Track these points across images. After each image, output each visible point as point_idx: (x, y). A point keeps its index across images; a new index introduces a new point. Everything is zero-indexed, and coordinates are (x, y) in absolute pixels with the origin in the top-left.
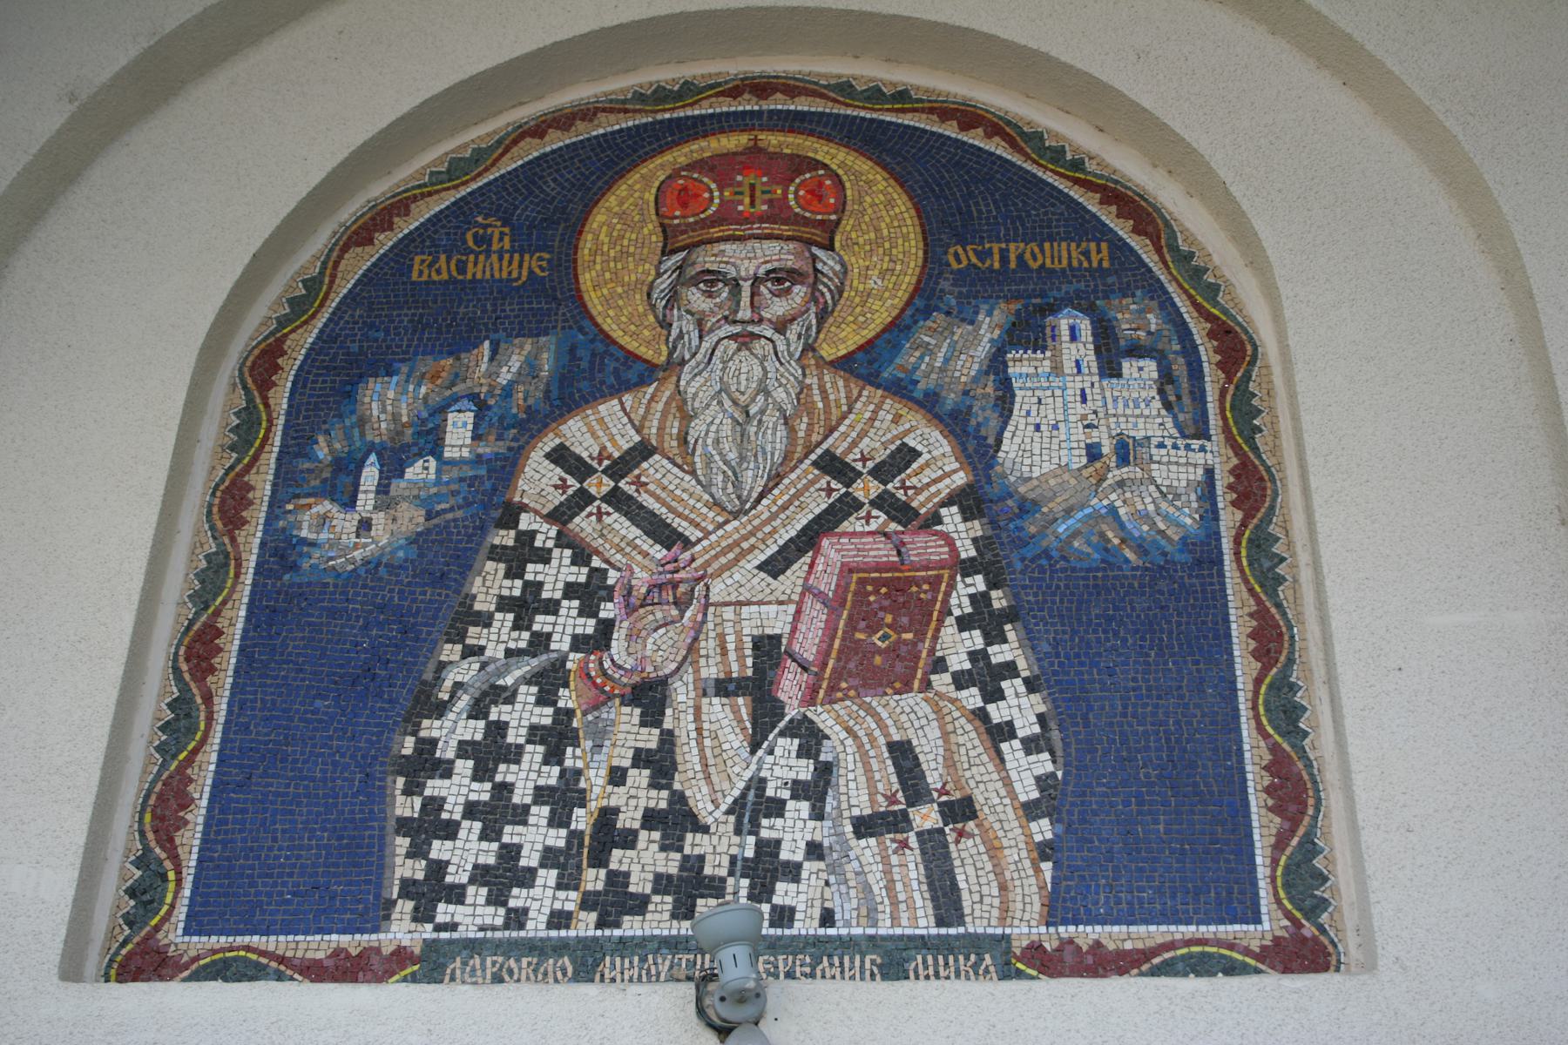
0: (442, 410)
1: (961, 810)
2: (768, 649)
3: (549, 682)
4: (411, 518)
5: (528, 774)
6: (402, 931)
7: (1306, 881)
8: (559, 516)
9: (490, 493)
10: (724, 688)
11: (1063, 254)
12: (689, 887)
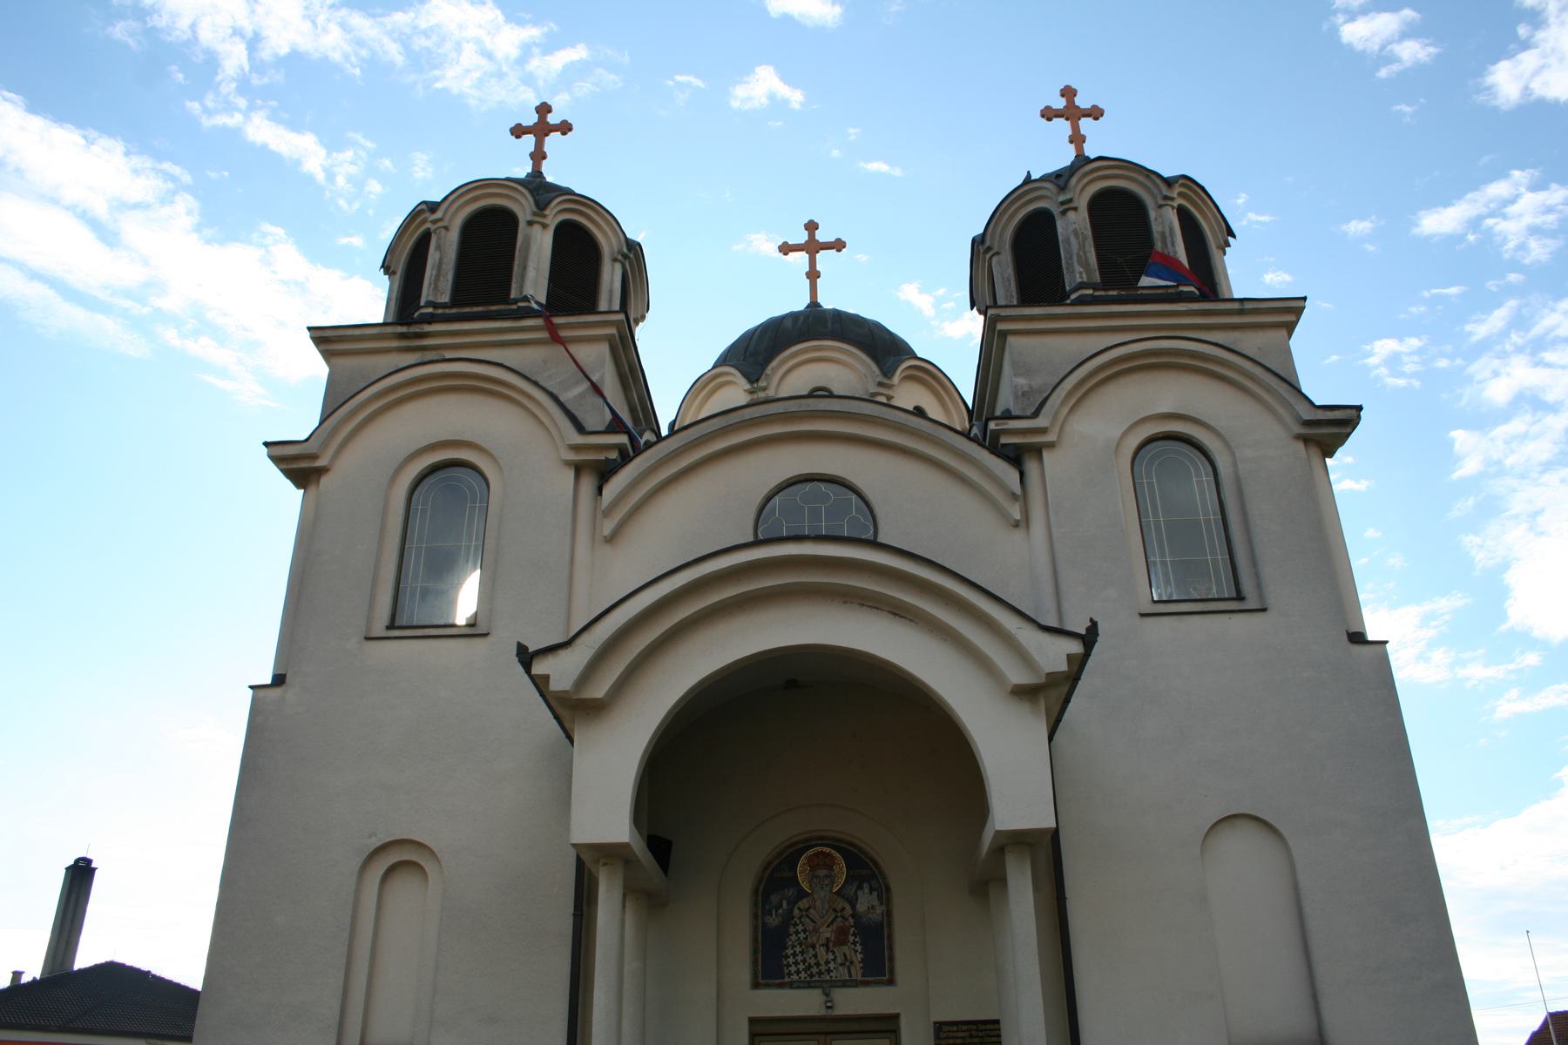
5: (799, 958)
7: (892, 971)
9: (788, 919)
12: (820, 973)
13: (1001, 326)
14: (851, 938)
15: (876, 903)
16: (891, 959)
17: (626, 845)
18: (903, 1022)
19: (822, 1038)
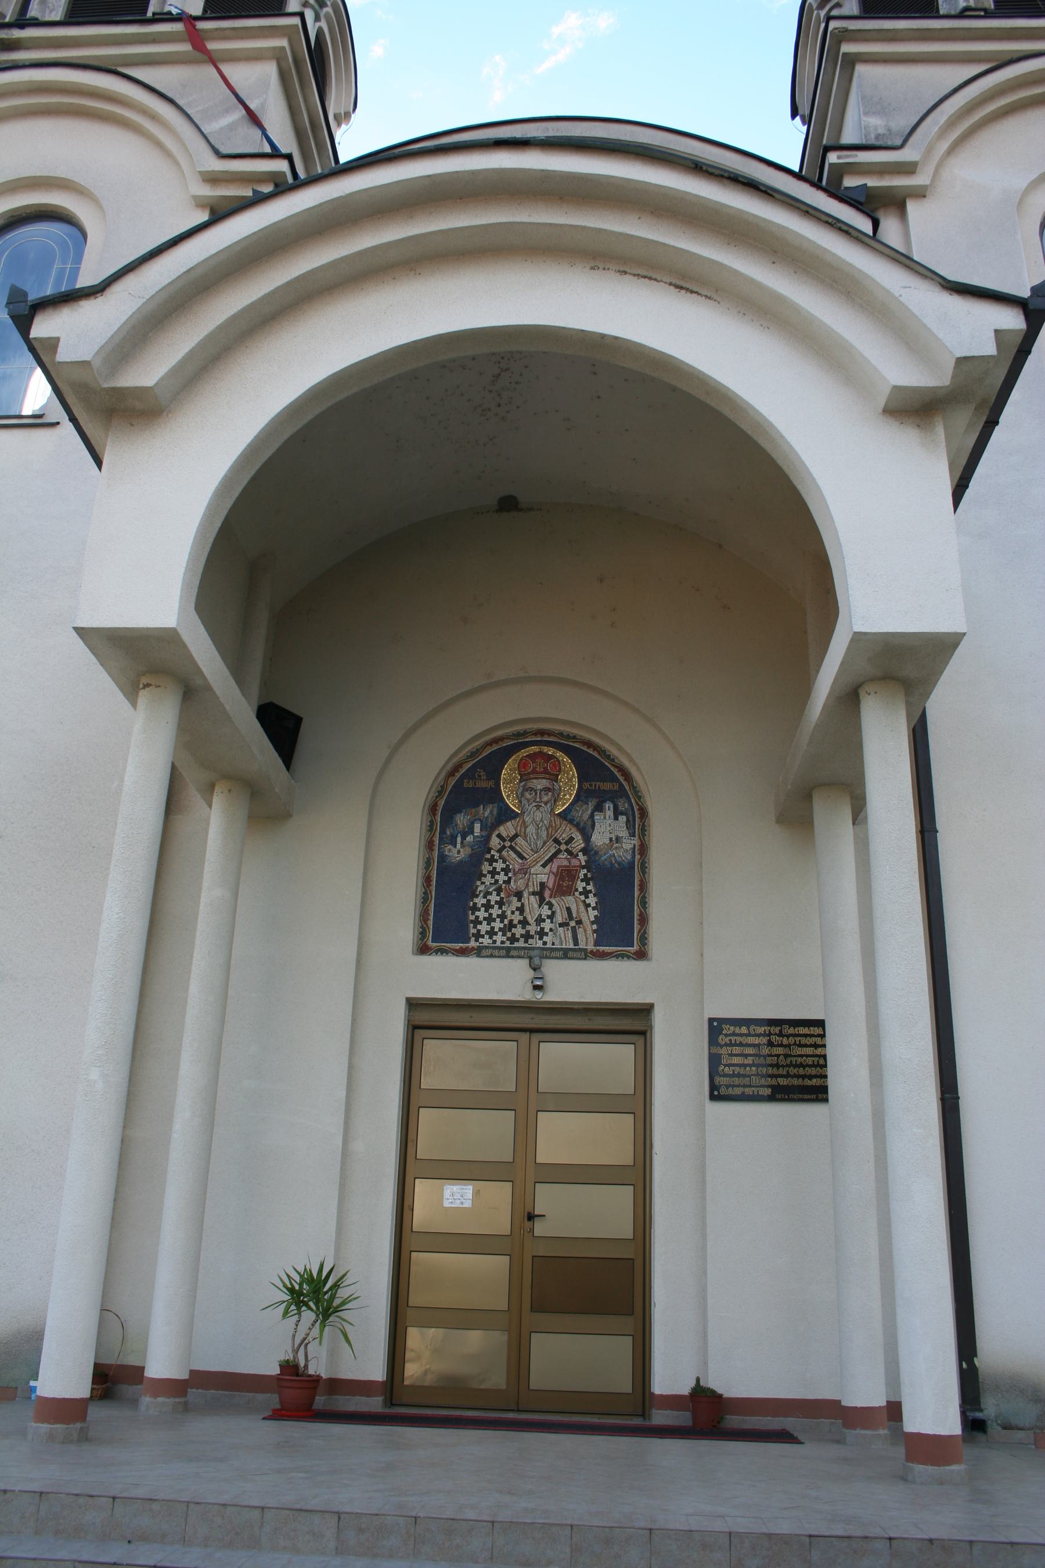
0: (473, 823)
1: (579, 922)
2: (543, 885)
3: (499, 891)
4: (468, 850)
5: (495, 912)
6: (473, 943)
7: (644, 939)
8: (500, 851)
9: (481, 852)
10: (534, 893)
11: (607, 786)
12: (527, 936)
13: (846, 48)
14: (580, 885)
15: (624, 833)
16: (644, 920)
17: (168, 638)
18: (659, 1021)
19: (524, 1037)
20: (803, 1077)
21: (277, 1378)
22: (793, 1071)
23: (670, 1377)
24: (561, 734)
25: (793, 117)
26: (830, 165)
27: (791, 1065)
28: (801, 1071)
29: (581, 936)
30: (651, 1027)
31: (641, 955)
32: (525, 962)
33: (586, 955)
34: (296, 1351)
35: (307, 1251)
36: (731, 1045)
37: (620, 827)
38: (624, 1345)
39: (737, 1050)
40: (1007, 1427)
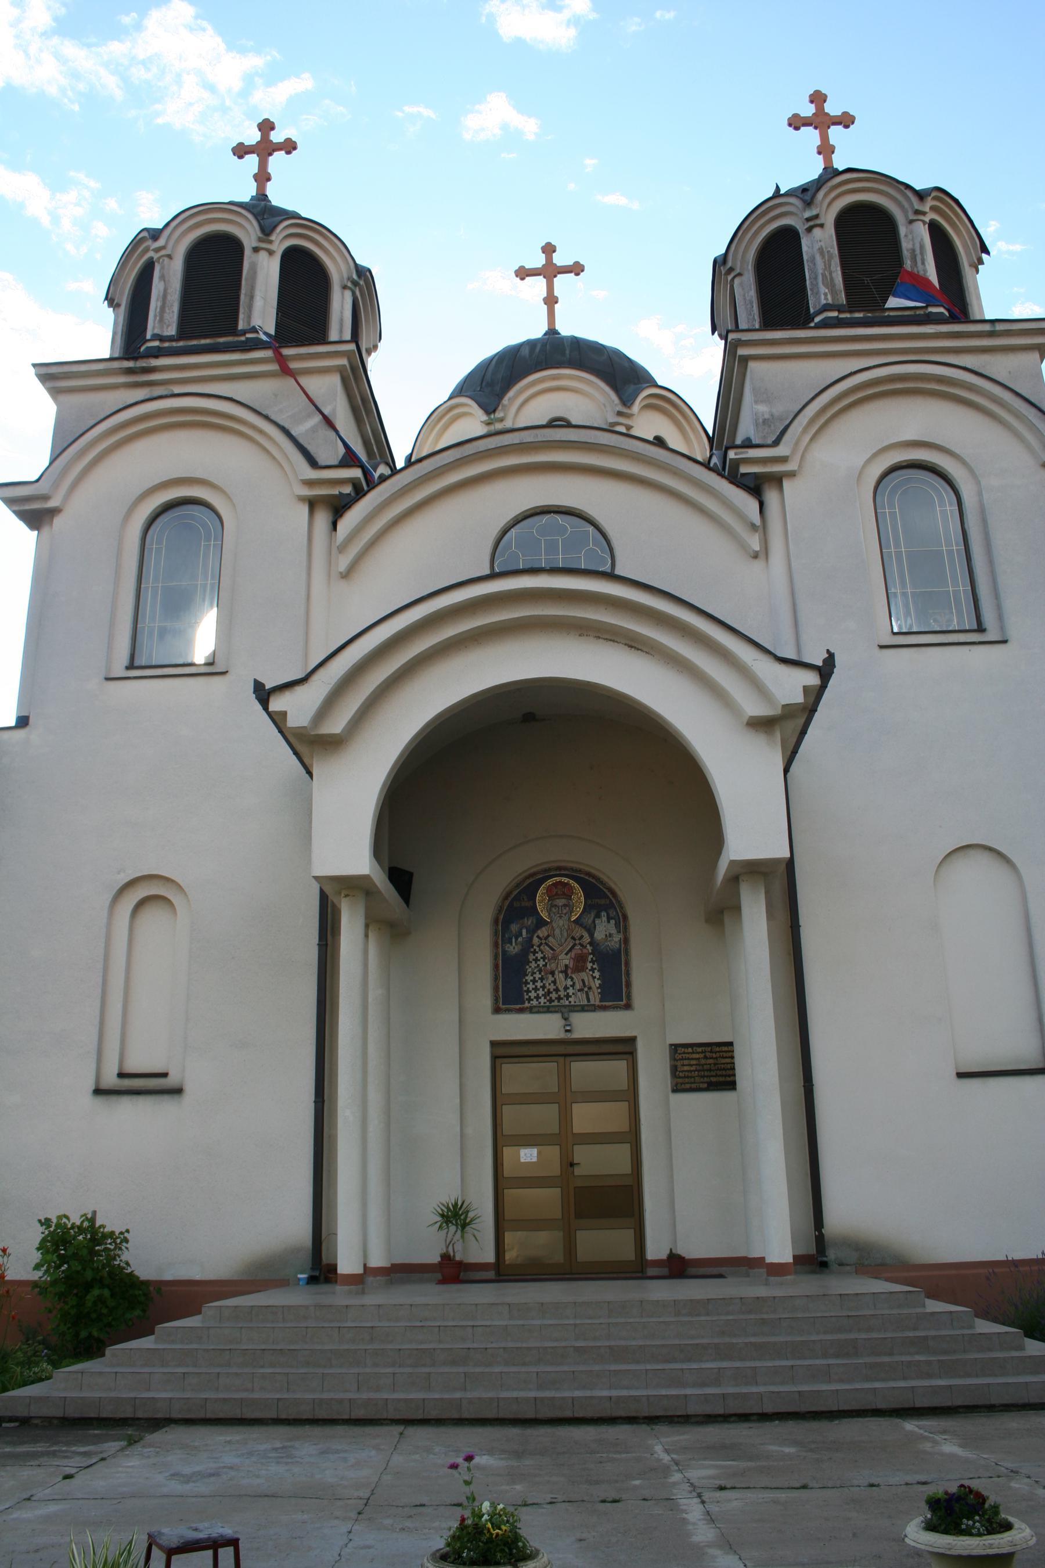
0: (521, 929)
1: (590, 988)
2: (566, 966)
3: (540, 971)
4: (520, 947)
5: (539, 984)
6: (527, 1005)
7: (629, 996)
8: (539, 946)
9: (528, 944)
10: (561, 972)
11: (602, 902)
12: (559, 999)
13: (742, 351)
14: (589, 965)
15: (614, 931)
16: (629, 985)
18: (640, 1045)
19: (561, 1059)
20: (726, 1076)
21: (440, 1263)
22: (719, 1073)
23: (656, 1249)
24: (572, 869)
25: (713, 333)
26: (731, 460)
27: (718, 1069)
28: (724, 1073)
29: (591, 997)
30: (636, 1050)
31: (628, 1006)
32: (558, 1016)
33: (594, 1008)
34: (447, 1247)
35: (446, 1193)
36: (682, 1059)
37: (611, 927)
38: (629, 1235)
39: (686, 1062)
40: (841, 1264)
